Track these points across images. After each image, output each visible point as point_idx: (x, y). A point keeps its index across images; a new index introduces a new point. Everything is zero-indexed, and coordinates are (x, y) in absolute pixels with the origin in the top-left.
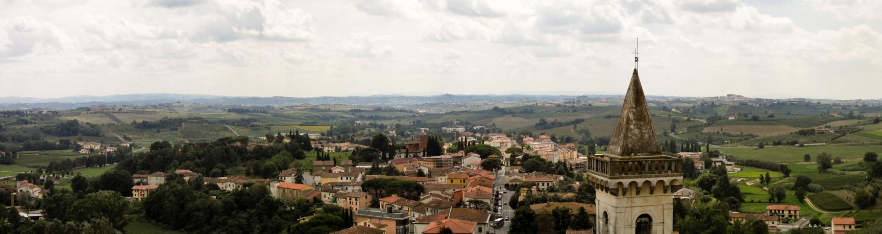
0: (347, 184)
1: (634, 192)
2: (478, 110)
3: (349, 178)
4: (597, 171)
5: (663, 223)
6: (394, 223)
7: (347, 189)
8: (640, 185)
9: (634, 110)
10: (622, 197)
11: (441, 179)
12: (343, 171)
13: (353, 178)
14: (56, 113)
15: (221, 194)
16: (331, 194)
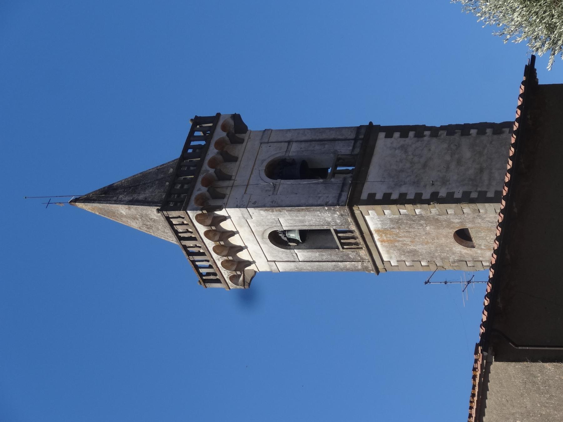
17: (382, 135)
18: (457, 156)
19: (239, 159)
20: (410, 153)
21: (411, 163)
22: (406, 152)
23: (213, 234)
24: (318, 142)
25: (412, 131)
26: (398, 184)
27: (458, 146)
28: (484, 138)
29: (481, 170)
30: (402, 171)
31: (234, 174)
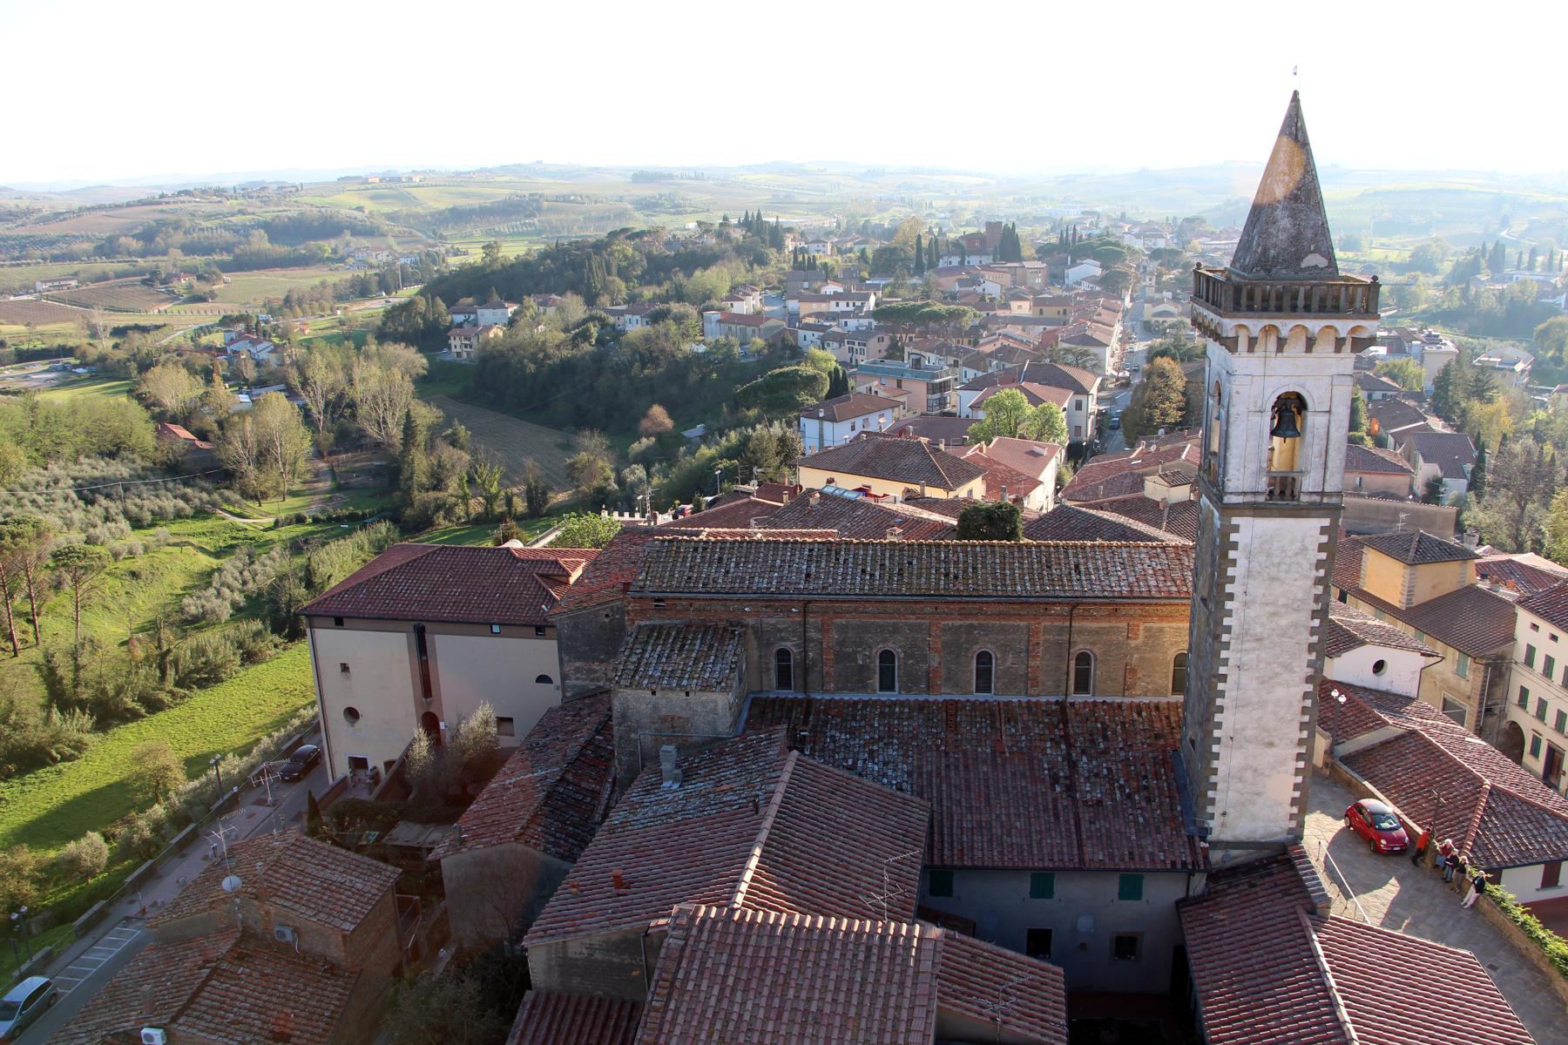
0: (845, 315)
1: (1272, 344)
2: (266, 272)
3: (851, 304)
4: (1207, 300)
5: (1329, 412)
6: (924, 388)
7: (846, 323)
8: (1284, 333)
10: (1246, 354)
11: (1020, 307)
12: (840, 290)
13: (858, 303)
14: (297, 189)
15: (232, 341)
16: (816, 334)
17: (1326, 522)
18: (1283, 610)
22: (1296, 554)
26: (1249, 556)
27: (1297, 610)
29: (1259, 640)
30: (1269, 555)
31: (1285, 354)
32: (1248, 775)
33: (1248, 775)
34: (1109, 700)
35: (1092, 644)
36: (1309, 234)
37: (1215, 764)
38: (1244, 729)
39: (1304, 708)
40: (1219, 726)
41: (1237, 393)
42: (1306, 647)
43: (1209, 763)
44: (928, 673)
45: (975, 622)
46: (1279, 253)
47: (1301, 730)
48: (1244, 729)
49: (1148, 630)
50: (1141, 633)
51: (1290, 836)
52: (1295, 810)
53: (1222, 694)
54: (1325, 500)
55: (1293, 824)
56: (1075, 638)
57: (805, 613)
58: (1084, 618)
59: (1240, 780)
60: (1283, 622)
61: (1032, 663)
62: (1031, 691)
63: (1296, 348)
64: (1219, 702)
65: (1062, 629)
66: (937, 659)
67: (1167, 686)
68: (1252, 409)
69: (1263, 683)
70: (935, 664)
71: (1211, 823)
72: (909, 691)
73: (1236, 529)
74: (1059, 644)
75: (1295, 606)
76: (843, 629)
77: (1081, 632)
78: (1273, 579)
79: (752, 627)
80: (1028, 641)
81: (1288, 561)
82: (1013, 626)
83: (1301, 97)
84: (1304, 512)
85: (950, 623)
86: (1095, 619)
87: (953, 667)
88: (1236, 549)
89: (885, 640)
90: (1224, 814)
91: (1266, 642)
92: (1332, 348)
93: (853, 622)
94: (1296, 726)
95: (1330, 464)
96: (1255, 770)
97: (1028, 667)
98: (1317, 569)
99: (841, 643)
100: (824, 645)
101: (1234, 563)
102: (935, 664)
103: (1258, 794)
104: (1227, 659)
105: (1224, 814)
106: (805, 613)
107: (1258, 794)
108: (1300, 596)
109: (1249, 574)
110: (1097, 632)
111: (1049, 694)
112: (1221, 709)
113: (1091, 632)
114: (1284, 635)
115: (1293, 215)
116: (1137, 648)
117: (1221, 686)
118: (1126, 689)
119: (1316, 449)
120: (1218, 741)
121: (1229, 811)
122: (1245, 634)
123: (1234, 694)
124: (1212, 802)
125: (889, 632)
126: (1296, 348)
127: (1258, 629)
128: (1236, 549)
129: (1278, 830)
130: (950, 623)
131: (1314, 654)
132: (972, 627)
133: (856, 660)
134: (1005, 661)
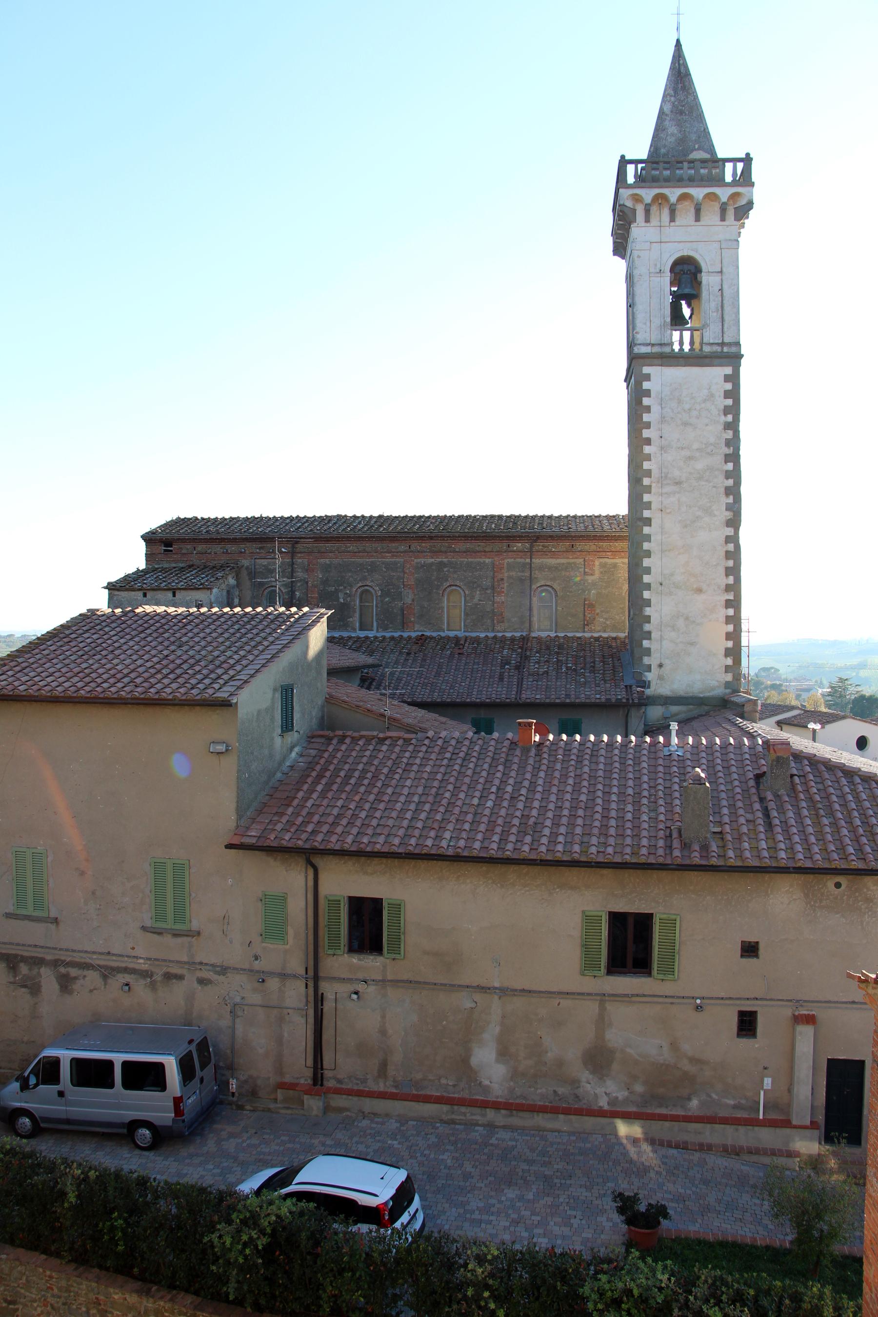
5: (721, 272)
9: (673, 99)
17: (728, 370)
18: (698, 454)
19: (698, 223)
20: (703, 405)
21: (689, 410)
22: (704, 401)
23: (358, 681)
24: (720, 304)
25: (630, 185)
26: (661, 402)
27: (711, 454)
28: (721, 477)
29: (678, 483)
30: (680, 402)
31: (677, 223)
32: (681, 623)
33: (681, 623)
34: (569, 635)
35: (551, 579)
36: (694, 137)
37: (648, 611)
38: (672, 575)
39: (727, 552)
40: (648, 571)
41: (639, 257)
42: (722, 490)
43: (641, 610)
44: (402, 610)
45: (445, 560)
46: (668, 152)
47: (727, 575)
48: (672, 575)
49: (603, 566)
50: (597, 568)
51: (728, 691)
52: (729, 661)
53: (648, 538)
54: (725, 349)
55: (729, 677)
56: (536, 574)
57: (293, 554)
58: (545, 553)
59: (674, 628)
60: (700, 465)
61: (497, 599)
62: (498, 628)
63: (686, 216)
64: (646, 546)
65: (524, 565)
66: (411, 596)
67: (624, 622)
68: (652, 270)
69: (686, 526)
70: (409, 600)
71: (649, 676)
72: (385, 629)
73: (648, 377)
74: (522, 580)
75: (709, 450)
76: (327, 568)
77: (541, 568)
78: (686, 424)
79: (247, 568)
80: (493, 578)
81: (698, 407)
82: (479, 563)
83: (682, 43)
84: (707, 361)
85: (422, 561)
86: (554, 555)
87: (426, 604)
88: (649, 396)
89: (364, 579)
90: (660, 666)
91: (685, 485)
92: (717, 218)
93: (336, 561)
94: (722, 571)
95: (726, 318)
96: (687, 619)
97: (494, 602)
98: (725, 415)
99: (325, 582)
100: (310, 584)
101: (648, 409)
102: (409, 600)
103: (692, 644)
104: (650, 503)
105: (660, 666)
106: (293, 554)
107: (692, 644)
108: (712, 440)
109: (663, 419)
110: (556, 568)
111: (515, 630)
112: (648, 554)
113: (550, 568)
114: (700, 478)
115: (679, 124)
116: (594, 584)
117: (646, 530)
118: (586, 624)
119: (713, 305)
120: (648, 587)
121: (666, 662)
122: (664, 478)
123: (659, 537)
124: (648, 652)
125: (368, 571)
126: (686, 216)
127: (676, 473)
128: (649, 396)
129: (714, 683)
130: (422, 561)
131: (731, 497)
132: (441, 565)
133: (338, 598)
134: (473, 597)
